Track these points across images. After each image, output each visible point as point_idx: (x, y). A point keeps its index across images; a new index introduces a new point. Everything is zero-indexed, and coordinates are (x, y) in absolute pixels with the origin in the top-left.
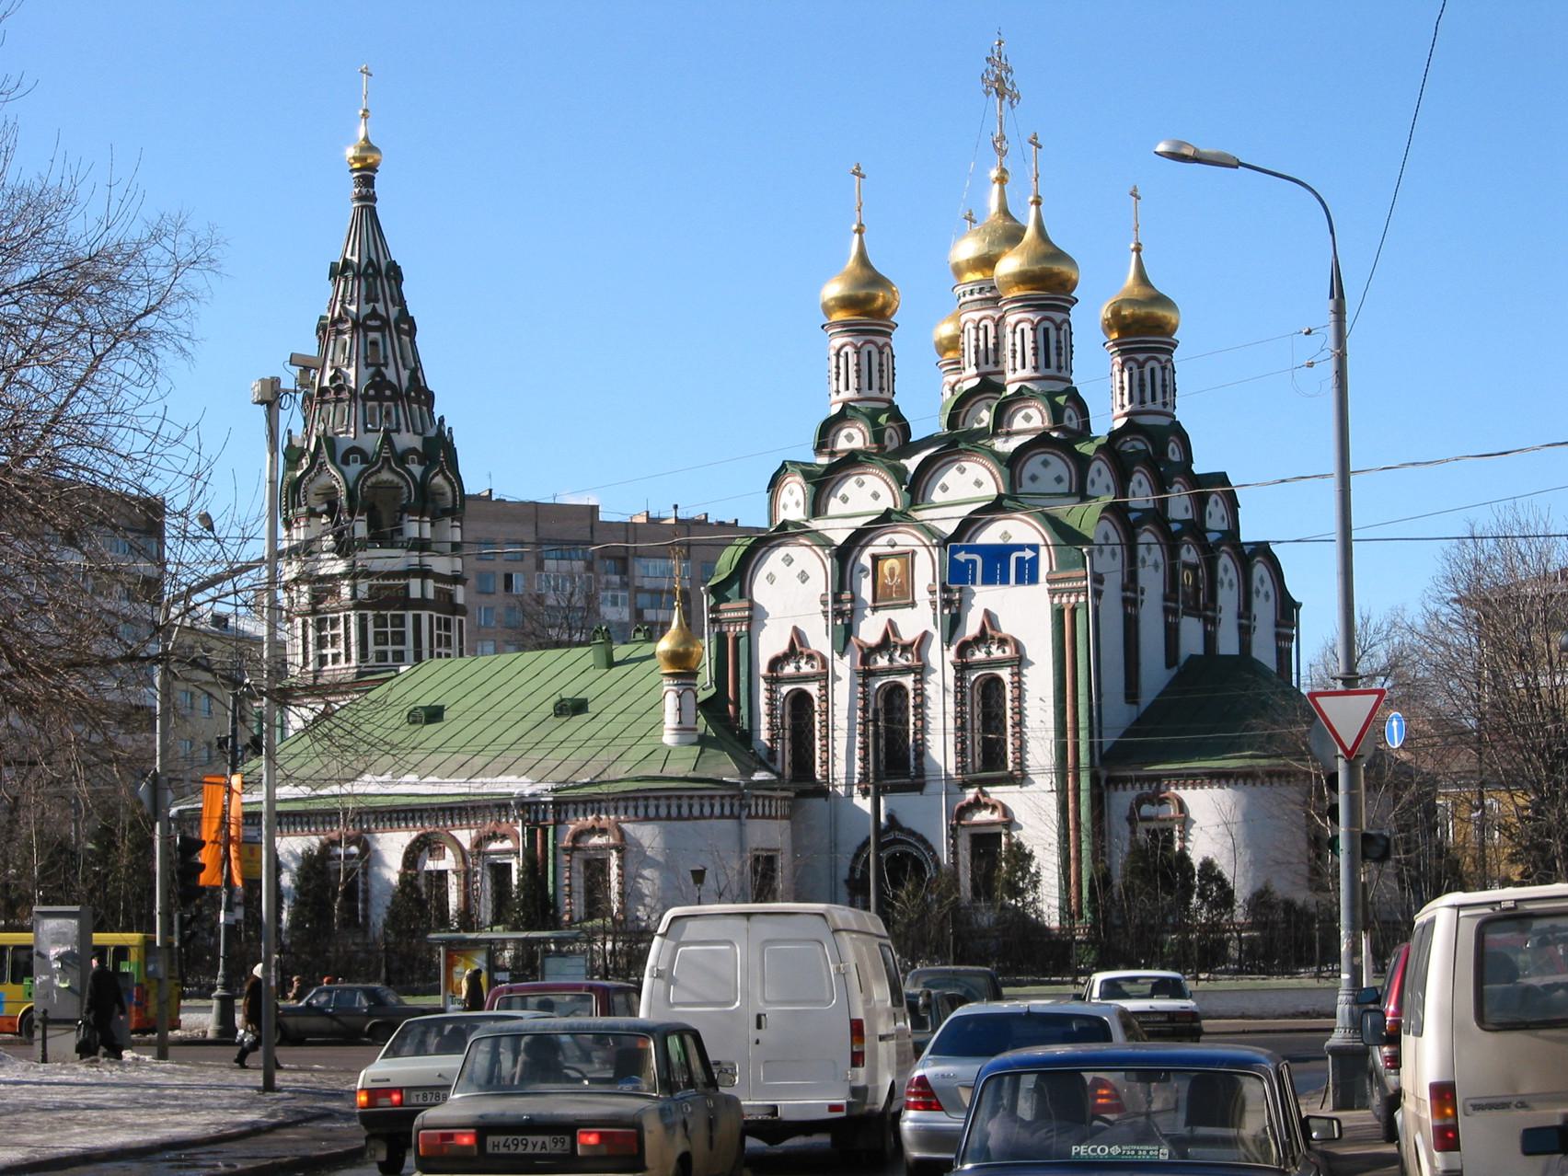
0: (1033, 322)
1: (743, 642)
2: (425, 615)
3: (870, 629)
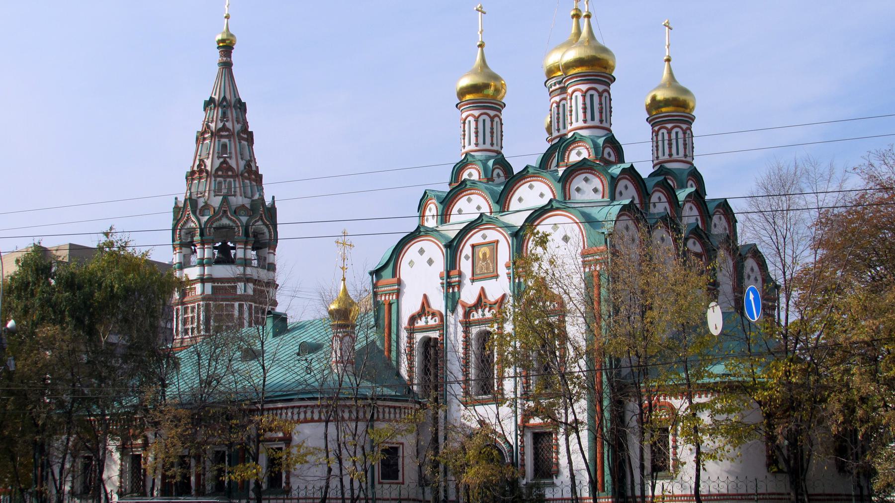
0: (582, 91)
1: (394, 307)
3: (469, 294)
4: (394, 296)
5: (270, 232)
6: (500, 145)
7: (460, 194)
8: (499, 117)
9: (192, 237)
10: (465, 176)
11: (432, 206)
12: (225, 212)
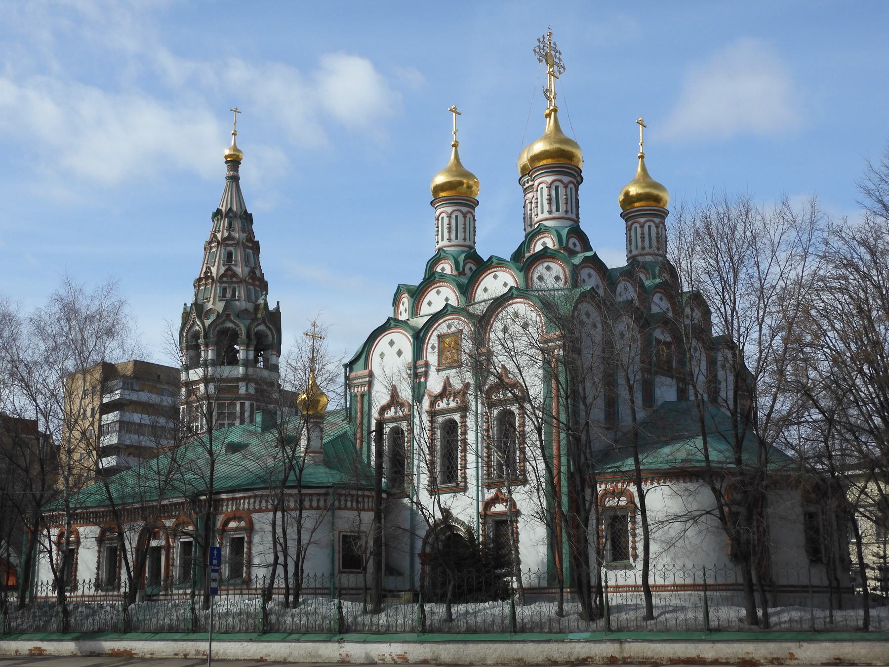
1: (366, 398)
2: (247, 403)
4: (366, 388)
5: (273, 334)
6: (472, 240)
7: (429, 287)
8: (472, 214)
9: (197, 341)
10: (439, 269)
12: (228, 316)
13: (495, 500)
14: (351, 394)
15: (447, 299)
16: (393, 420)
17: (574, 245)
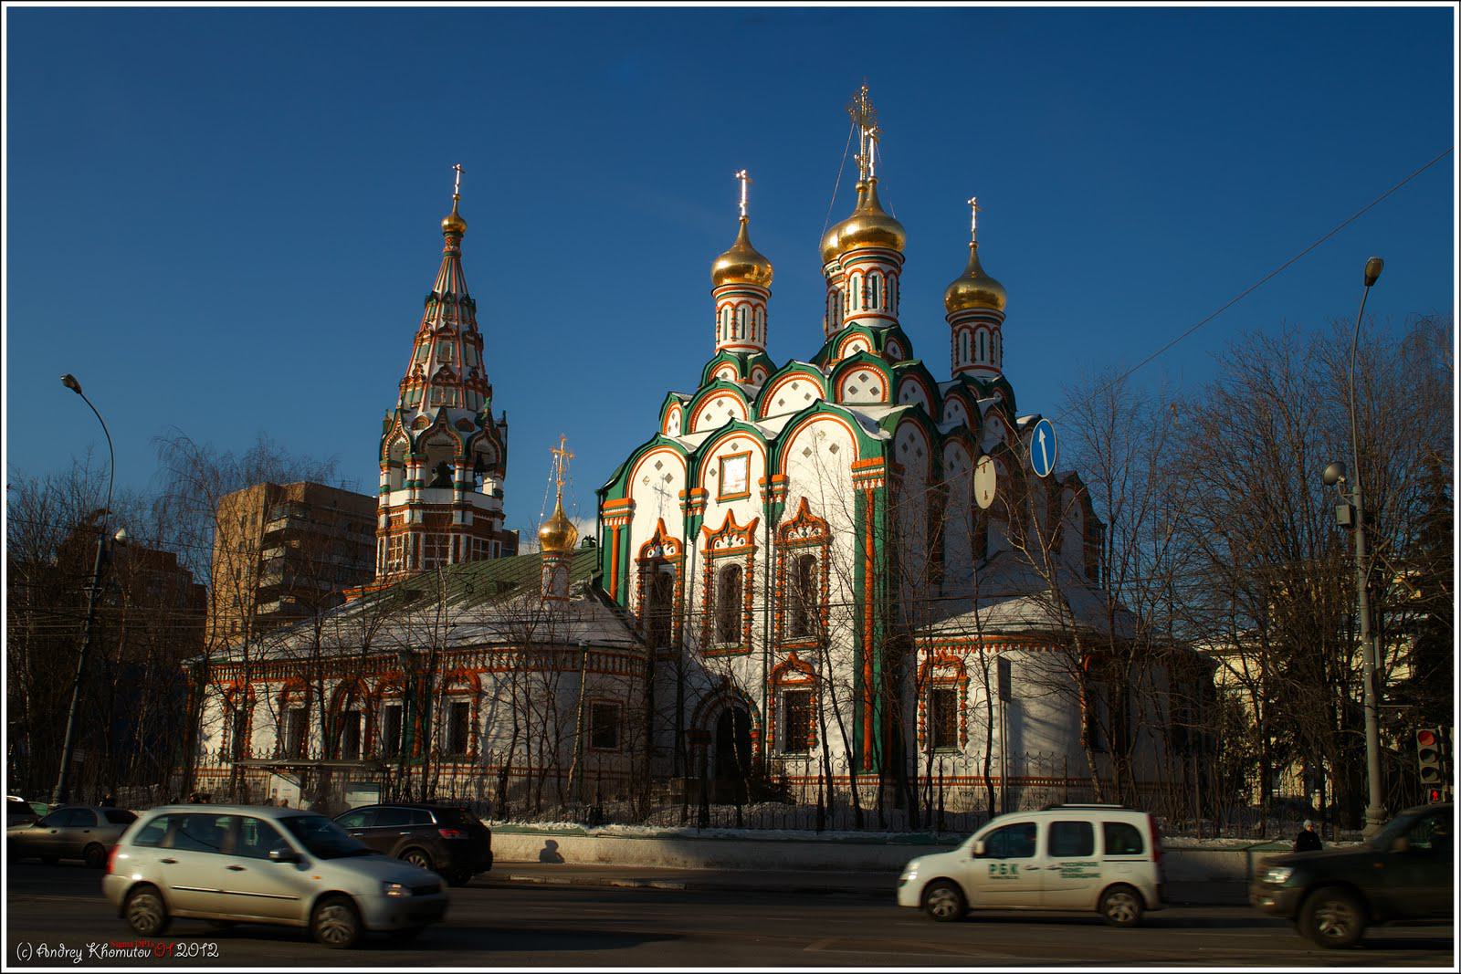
1: (624, 534)
2: (463, 537)
11: (676, 412)
12: (442, 426)
13: (790, 666)
14: (604, 527)
15: (731, 413)
16: (728, 553)
17: (894, 350)
